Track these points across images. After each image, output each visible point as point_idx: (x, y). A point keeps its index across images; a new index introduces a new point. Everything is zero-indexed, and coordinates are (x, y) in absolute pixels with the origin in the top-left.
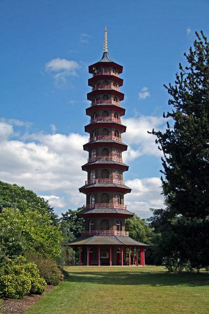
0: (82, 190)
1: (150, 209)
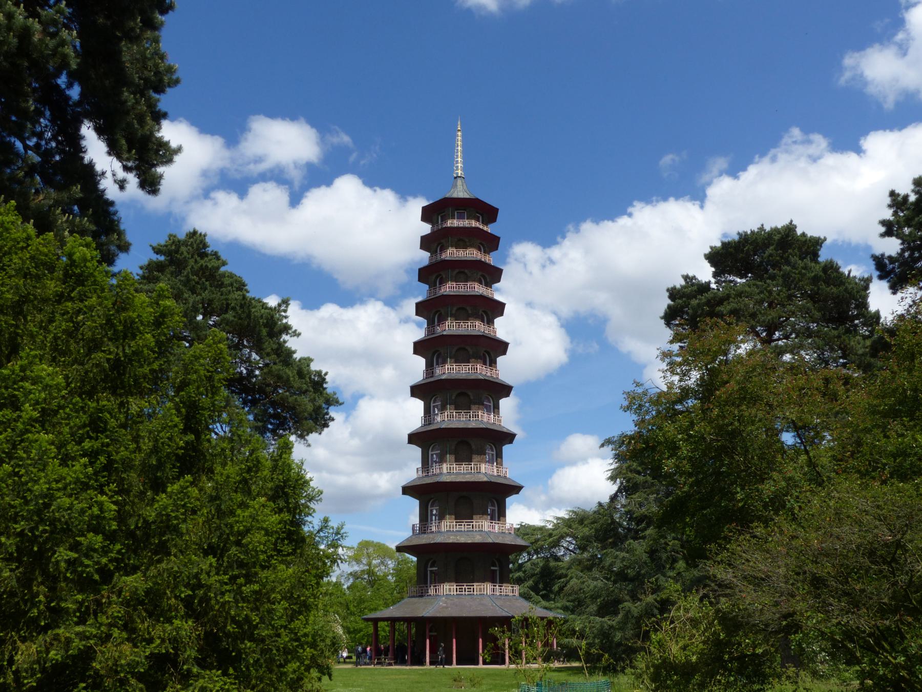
0: (408, 490)
1: (602, 445)
